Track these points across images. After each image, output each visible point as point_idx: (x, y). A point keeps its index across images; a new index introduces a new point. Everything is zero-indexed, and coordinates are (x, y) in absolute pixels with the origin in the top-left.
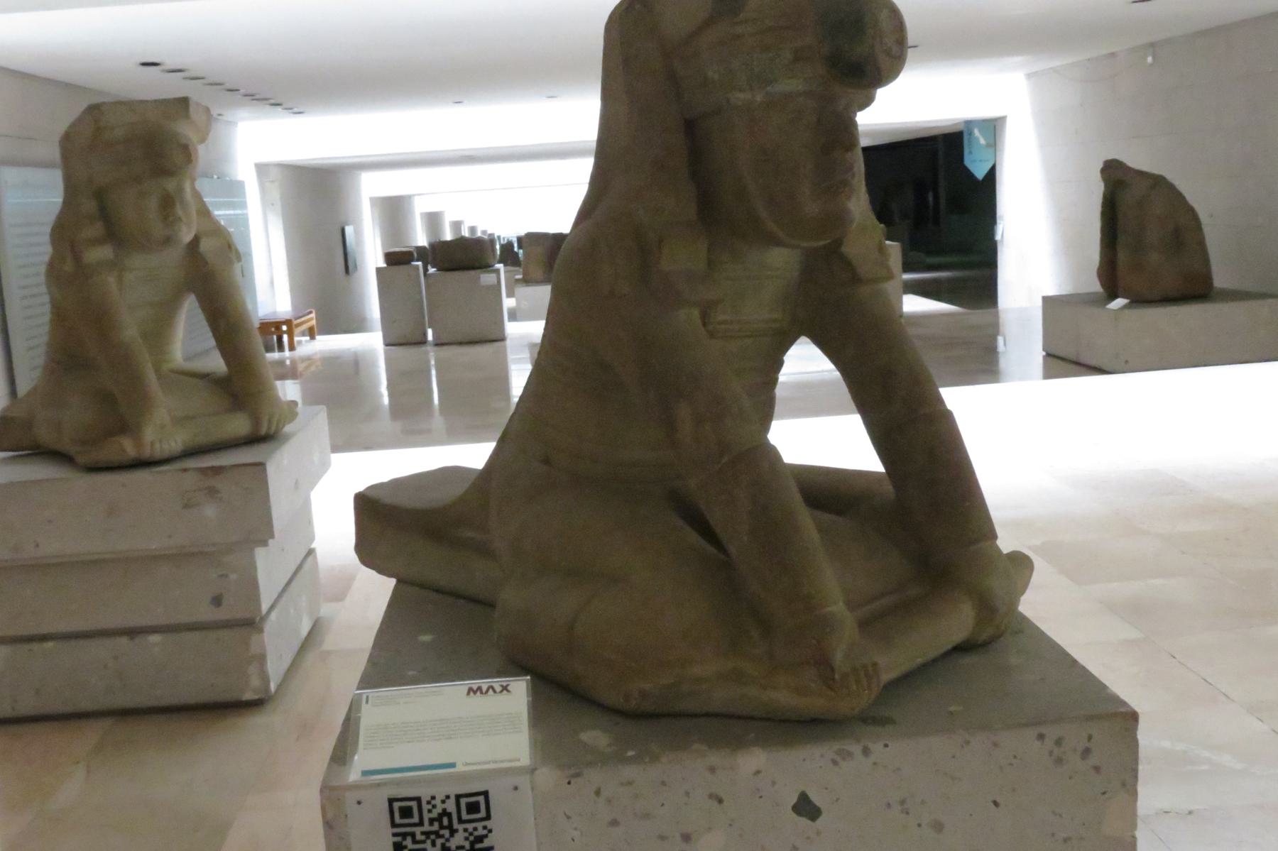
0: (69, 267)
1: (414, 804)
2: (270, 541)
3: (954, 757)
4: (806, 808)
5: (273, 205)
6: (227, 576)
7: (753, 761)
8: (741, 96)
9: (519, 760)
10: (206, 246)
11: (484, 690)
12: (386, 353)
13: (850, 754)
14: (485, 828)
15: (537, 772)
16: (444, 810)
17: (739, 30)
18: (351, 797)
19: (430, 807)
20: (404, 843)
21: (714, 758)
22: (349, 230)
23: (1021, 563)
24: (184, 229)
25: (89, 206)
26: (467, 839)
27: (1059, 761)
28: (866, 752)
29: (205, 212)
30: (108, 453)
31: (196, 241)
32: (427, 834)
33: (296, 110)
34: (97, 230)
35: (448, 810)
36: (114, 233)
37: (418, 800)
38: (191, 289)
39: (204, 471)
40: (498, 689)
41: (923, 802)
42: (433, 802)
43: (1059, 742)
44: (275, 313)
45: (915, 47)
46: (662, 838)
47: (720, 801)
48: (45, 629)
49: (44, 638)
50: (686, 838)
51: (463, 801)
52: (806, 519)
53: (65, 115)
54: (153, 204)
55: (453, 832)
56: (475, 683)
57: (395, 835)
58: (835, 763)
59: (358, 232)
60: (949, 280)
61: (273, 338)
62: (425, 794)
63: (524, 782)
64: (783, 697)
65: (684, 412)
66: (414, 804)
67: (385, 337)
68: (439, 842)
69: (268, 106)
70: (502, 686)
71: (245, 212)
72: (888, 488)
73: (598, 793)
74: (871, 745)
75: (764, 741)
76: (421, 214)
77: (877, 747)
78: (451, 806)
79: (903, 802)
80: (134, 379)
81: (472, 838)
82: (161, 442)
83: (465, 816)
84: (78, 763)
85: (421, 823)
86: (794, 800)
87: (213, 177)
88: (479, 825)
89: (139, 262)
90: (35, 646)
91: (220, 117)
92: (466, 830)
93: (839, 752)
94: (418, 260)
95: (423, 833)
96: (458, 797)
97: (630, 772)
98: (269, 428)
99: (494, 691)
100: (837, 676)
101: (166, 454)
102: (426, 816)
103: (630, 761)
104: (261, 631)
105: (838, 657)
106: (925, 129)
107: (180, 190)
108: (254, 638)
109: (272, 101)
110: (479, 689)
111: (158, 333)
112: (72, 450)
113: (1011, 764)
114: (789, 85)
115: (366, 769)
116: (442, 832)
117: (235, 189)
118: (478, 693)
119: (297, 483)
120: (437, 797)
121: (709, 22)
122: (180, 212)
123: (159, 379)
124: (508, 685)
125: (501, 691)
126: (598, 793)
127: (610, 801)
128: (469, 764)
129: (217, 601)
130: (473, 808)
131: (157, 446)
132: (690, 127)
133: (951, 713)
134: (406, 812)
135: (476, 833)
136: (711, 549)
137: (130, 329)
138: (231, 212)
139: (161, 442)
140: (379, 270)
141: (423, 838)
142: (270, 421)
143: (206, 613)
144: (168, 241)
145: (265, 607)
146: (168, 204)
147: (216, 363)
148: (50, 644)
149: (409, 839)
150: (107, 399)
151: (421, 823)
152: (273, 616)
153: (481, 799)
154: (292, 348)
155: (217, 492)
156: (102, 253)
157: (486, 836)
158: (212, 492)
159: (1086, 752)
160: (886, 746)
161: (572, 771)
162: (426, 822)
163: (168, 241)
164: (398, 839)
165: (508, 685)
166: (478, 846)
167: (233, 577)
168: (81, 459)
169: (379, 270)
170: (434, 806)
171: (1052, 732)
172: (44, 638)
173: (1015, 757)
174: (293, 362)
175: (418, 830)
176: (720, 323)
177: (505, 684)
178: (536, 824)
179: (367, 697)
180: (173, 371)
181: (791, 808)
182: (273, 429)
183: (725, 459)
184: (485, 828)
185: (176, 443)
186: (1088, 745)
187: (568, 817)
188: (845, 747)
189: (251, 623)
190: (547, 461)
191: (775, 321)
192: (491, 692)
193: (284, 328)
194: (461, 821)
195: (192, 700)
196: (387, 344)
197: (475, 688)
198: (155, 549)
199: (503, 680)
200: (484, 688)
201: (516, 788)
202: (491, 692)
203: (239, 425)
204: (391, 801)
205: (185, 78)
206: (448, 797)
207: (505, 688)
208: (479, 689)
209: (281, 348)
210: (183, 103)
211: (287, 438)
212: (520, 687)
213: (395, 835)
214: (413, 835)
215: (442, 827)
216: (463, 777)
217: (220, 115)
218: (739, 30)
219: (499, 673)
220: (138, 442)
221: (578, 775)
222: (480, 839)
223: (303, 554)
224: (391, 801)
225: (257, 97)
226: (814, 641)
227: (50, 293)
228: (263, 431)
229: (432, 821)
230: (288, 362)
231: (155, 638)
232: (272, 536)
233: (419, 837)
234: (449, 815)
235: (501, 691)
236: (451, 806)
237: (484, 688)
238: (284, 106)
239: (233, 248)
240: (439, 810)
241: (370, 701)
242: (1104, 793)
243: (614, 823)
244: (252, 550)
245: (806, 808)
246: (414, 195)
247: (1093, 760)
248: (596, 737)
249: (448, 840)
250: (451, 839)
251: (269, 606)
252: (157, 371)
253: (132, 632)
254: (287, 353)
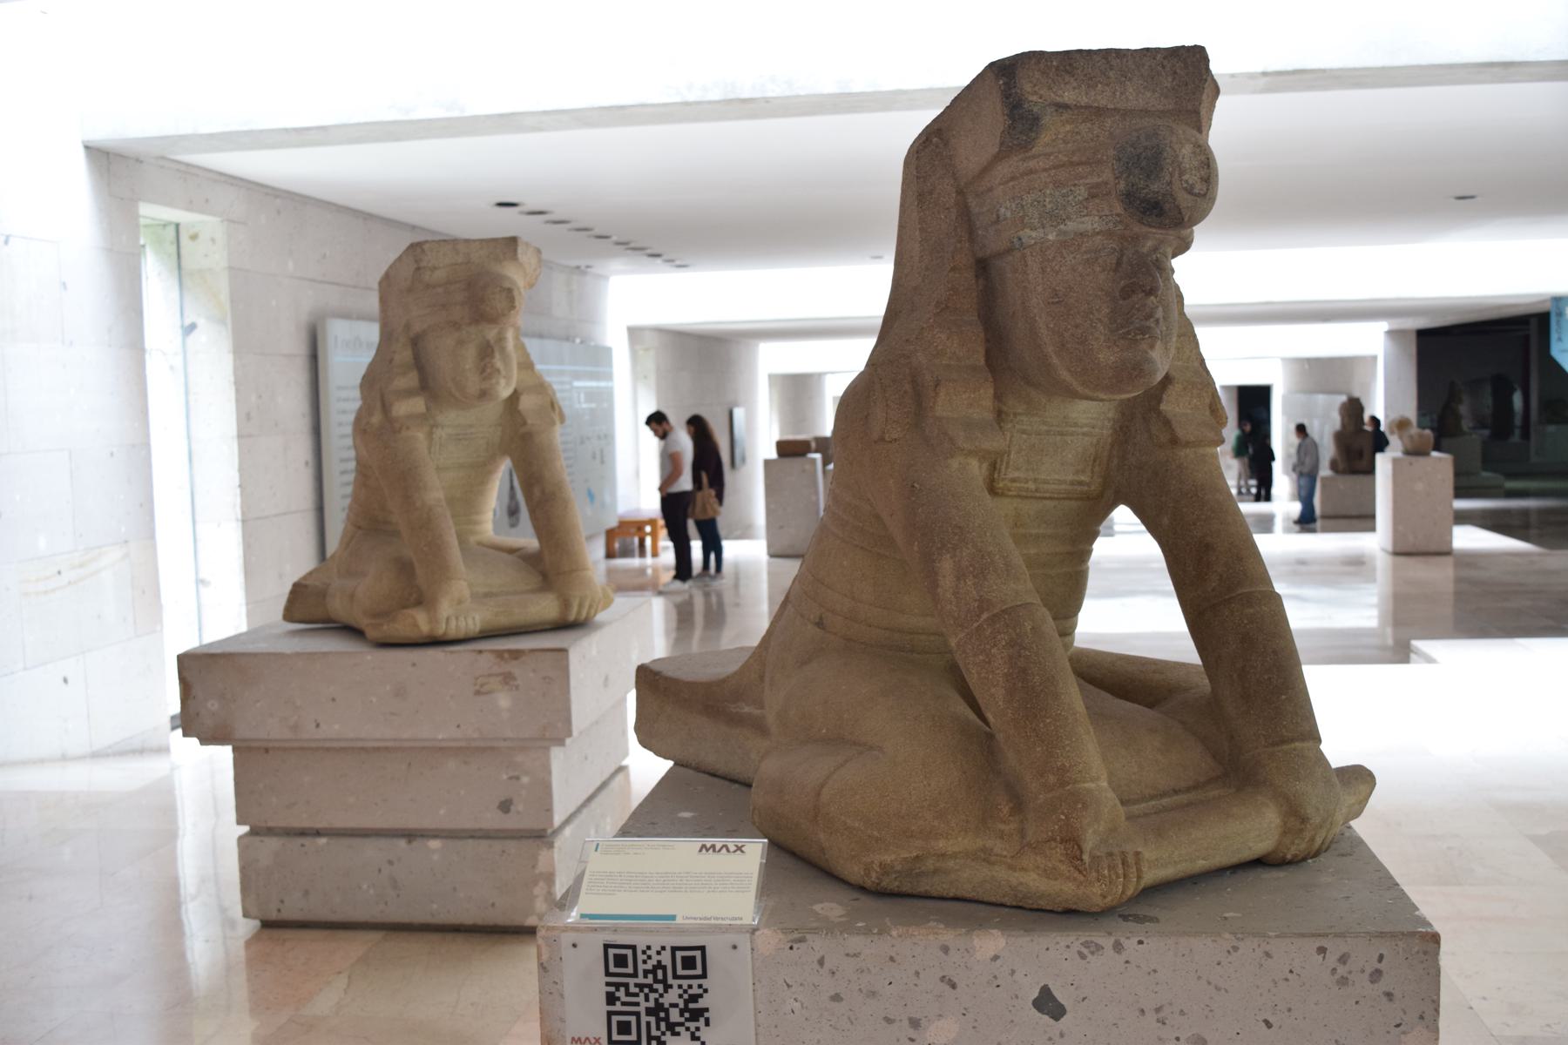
0: (376, 419)
1: (629, 952)
2: (568, 741)
3: (1219, 964)
4: (1047, 1004)
5: (645, 377)
6: (518, 778)
7: (990, 943)
8: (1034, 234)
9: (741, 919)
10: (527, 403)
11: (717, 848)
12: (769, 564)
13: (1099, 948)
14: (700, 986)
15: (757, 933)
16: (659, 962)
17: (1032, 164)
18: (567, 938)
19: (645, 957)
20: (617, 994)
21: (948, 936)
22: (739, 414)
23: (1359, 778)
24: (503, 382)
25: (404, 355)
26: (680, 996)
27: (1343, 982)
28: (1118, 947)
29: (527, 365)
30: (399, 628)
31: (515, 397)
32: (641, 986)
33: (678, 263)
34: (411, 380)
35: (663, 964)
36: (426, 386)
37: (633, 948)
38: (504, 449)
39: (499, 654)
40: (732, 848)
41: (1182, 1012)
42: (649, 952)
43: (1343, 959)
44: (638, 510)
45: (1472, 197)
46: (888, 1020)
47: (954, 986)
48: (320, 824)
49: (318, 833)
50: (915, 1023)
51: (679, 954)
52: (1073, 694)
53: (387, 253)
54: (470, 354)
55: (667, 987)
56: (709, 841)
57: (608, 984)
58: (1082, 956)
59: (751, 418)
60: (1542, 512)
61: (633, 543)
62: (641, 942)
63: (744, 942)
64: (1033, 881)
65: (946, 565)
66: (629, 952)
67: (769, 547)
68: (653, 996)
69: (645, 257)
70: (736, 846)
71: (610, 384)
72: (1205, 683)
73: (821, 962)
74: (1122, 940)
75: (1005, 926)
76: (771, 377)
77: (1130, 944)
78: (666, 958)
79: (1158, 1010)
80: (435, 551)
81: (686, 996)
82: (457, 618)
83: (680, 972)
84: (340, 973)
85: (635, 975)
86: (1036, 994)
87: (574, 341)
88: (695, 983)
89: (451, 419)
90: (307, 841)
91: (589, 270)
92: (680, 987)
93: (1086, 944)
94: (816, 451)
95: (636, 985)
96: (674, 949)
97: (855, 942)
98: (579, 612)
99: (728, 850)
100: (1086, 857)
101: (461, 635)
102: (641, 967)
103: (859, 932)
104: (551, 846)
105: (1090, 842)
106: (1500, 307)
107: (501, 339)
108: (543, 854)
109: (649, 251)
110: (713, 847)
111: (466, 501)
112: (363, 622)
113: (1287, 980)
114: (1090, 223)
115: (584, 913)
116: (655, 986)
117: (599, 358)
118: (711, 850)
119: (606, 679)
120: (652, 948)
121: (998, 158)
122: (499, 364)
123: (462, 550)
124: (743, 846)
125: (735, 851)
126: (821, 962)
127: (833, 973)
128: (689, 918)
129: (505, 806)
130: (689, 963)
131: (453, 623)
132: (983, 266)
133: (1226, 918)
134: (621, 961)
135: (690, 992)
136: (972, 716)
137: (435, 491)
138: (593, 384)
139: (457, 618)
140: (767, 463)
141: (637, 990)
142: (581, 606)
143: (492, 819)
144: (484, 395)
145: (558, 819)
146: (487, 352)
147: (526, 539)
148: (323, 841)
149: (622, 989)
150: (405, 568)
151: (635, 975)
152: (568, 831)
153: (698, 954)
154: (655, 554)
155: (514, 679)
156: (417, 404)
157: (701, 996)
158: (508, 678)
159: (1376, 975)
160: (1141, 942)
161: (796, 935)
162: (641, 973)
163: (484, 395)
164: (612, 989)
165: (743, 846)
166: (692, 1006)
167: (525, 780)
168: (371, 633)
169: (767, 463)
170: (649, 957)
171: (1336, 948)
172: (318, 833)
173: (1291, 972)
174: (655, 570)
175: (632, 981)
176: (1013, 480)
177: (740, 845)
178: (754, 990)
179: (598, 845)
180: (480, 543)
181: (1031, 1002)
182: (584, 615)
183: (985, 616)
184: (700, 986)
185: (474, 621)
186: (1379, 966)
187: (788, 986)
188: (1093, 939)
189: (541, 836)
190: (820, 624)
191: (1081, 483)
192: (724, 850)
193: (648, 529)
194: (675, 976)
195: (468, 918)
196: (772, 555)
197: (708, 845)
198: (443, 740)
199: (740, 841)
200: (718, 846)
201: (735, 947)
202: (724, 850)
203: (545, 607)
204: (607, 947)
205: (548, 222)
206: (663, 948)
207: (739, 849)
208: (713, 847)
209: (642, 553)
210: (511, 244)
211: (599, 626)
212: (756, 848)
213: (608, 984)
214: (626, 986)
215: (656, 981)
216: (682, 931)
217: (588, 267)
218: (1032, 164)
219: (732, 833)
220: (433, 620)
221: (801, 940)
222: (694, 998)
223: (612, 770)
224: (607, 947)
225: (632, 245)
226: (1063, 817)
227: (356, 447)
228: (572, 617)
229: (646, 973)
230: (649, 571)
231: (435, 844)
232: (570, 734)
233: (633, 989)
234: (664, 968)
235: (735, 851)
236: (666, 958)
237: (718, 846)
238: (665, 257)
239: (556, 406)
240: (655, 958)
241: (599, 850)
242: (1398, 1026)
243: (836, 998)
244: (547, 749)
245: (1047, 1004)
246: (825, 373)
247: (1383, 986)
248: (831, 907)
249: (661, 996)
250: (665, 995)
251: (563, 818)
252: (462, 540)
253: (410, 835)
254: (649, 560)
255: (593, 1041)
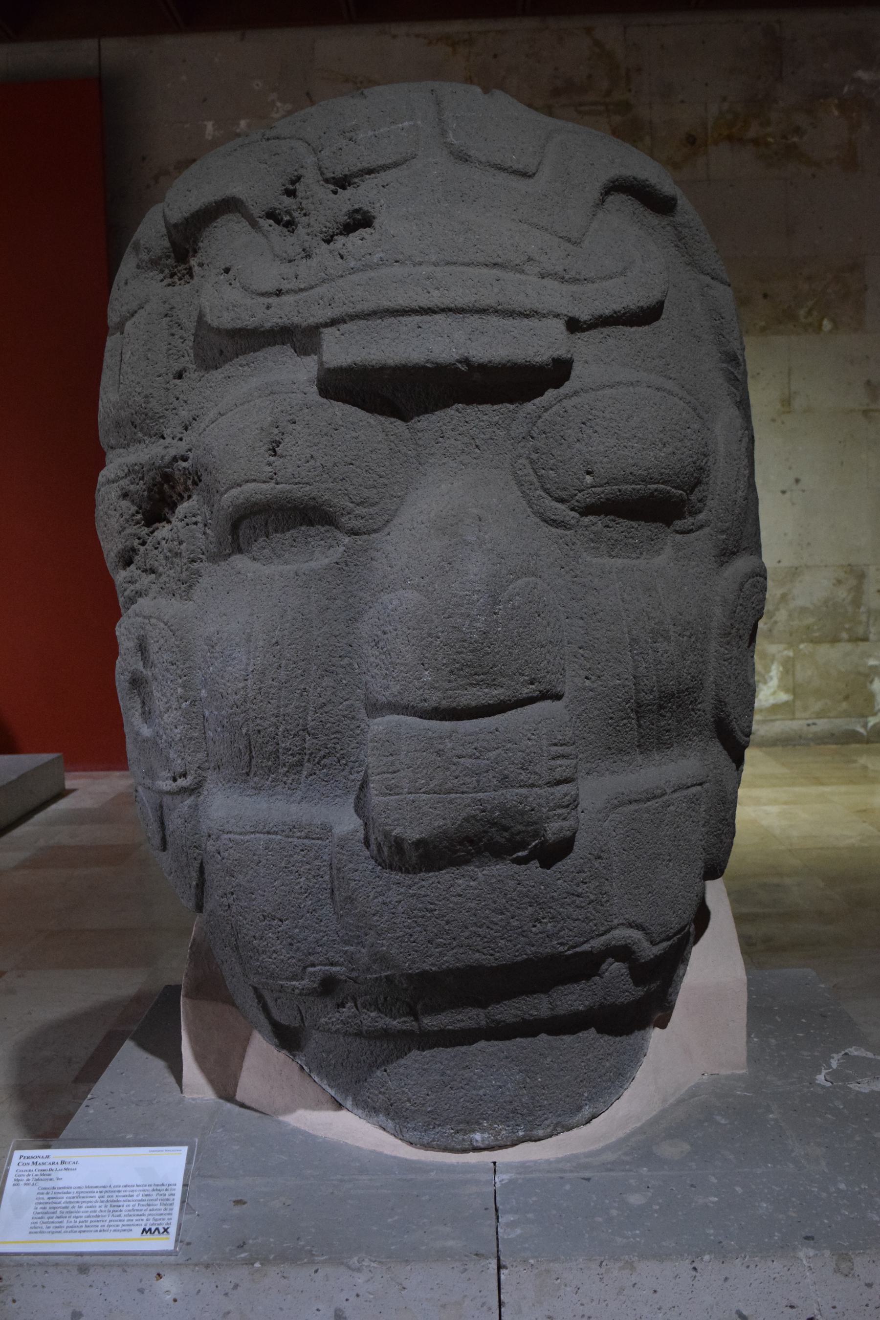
99: (159, 1232)
125: (163, 1233)
255: (162, 1230)
